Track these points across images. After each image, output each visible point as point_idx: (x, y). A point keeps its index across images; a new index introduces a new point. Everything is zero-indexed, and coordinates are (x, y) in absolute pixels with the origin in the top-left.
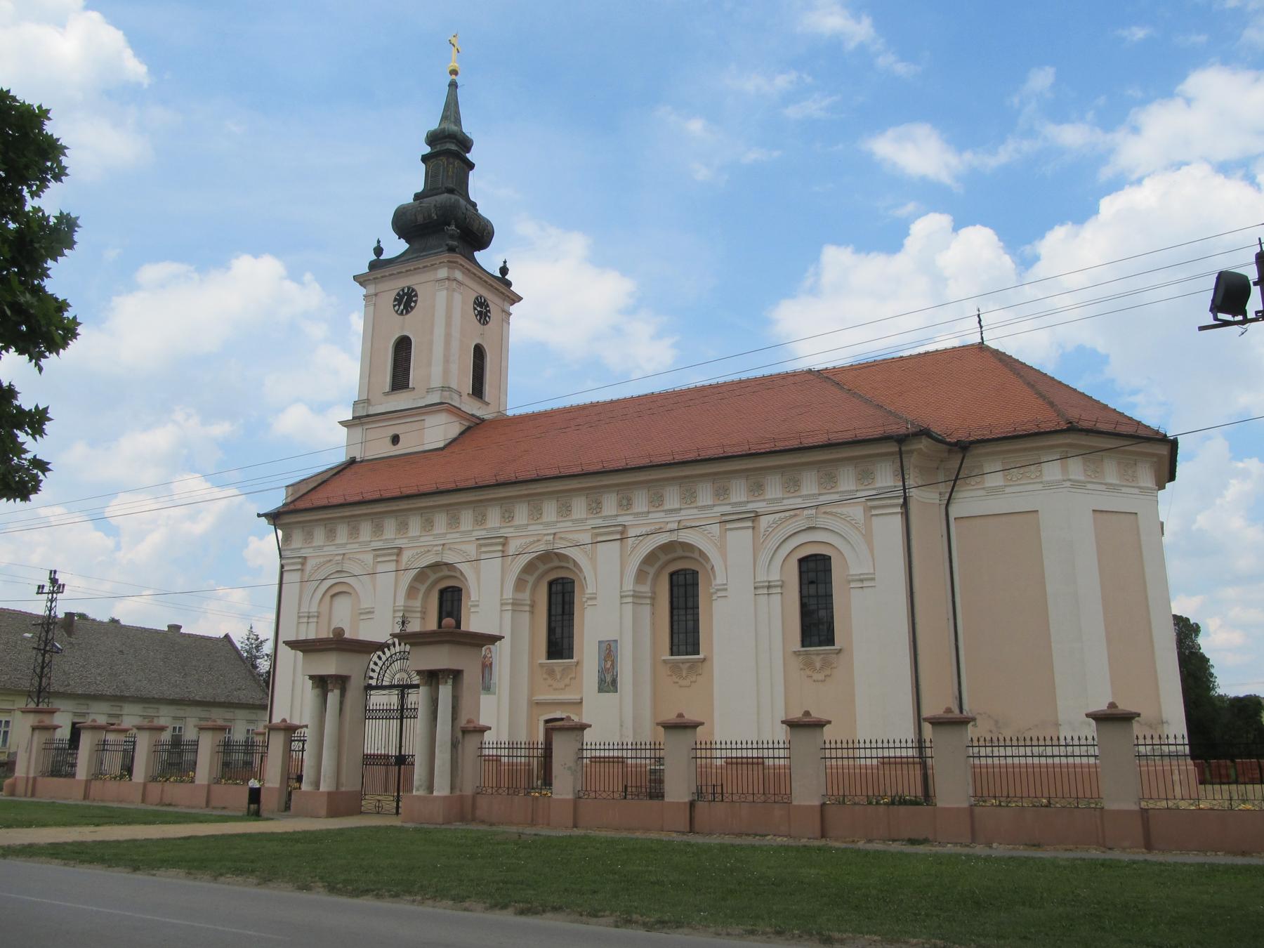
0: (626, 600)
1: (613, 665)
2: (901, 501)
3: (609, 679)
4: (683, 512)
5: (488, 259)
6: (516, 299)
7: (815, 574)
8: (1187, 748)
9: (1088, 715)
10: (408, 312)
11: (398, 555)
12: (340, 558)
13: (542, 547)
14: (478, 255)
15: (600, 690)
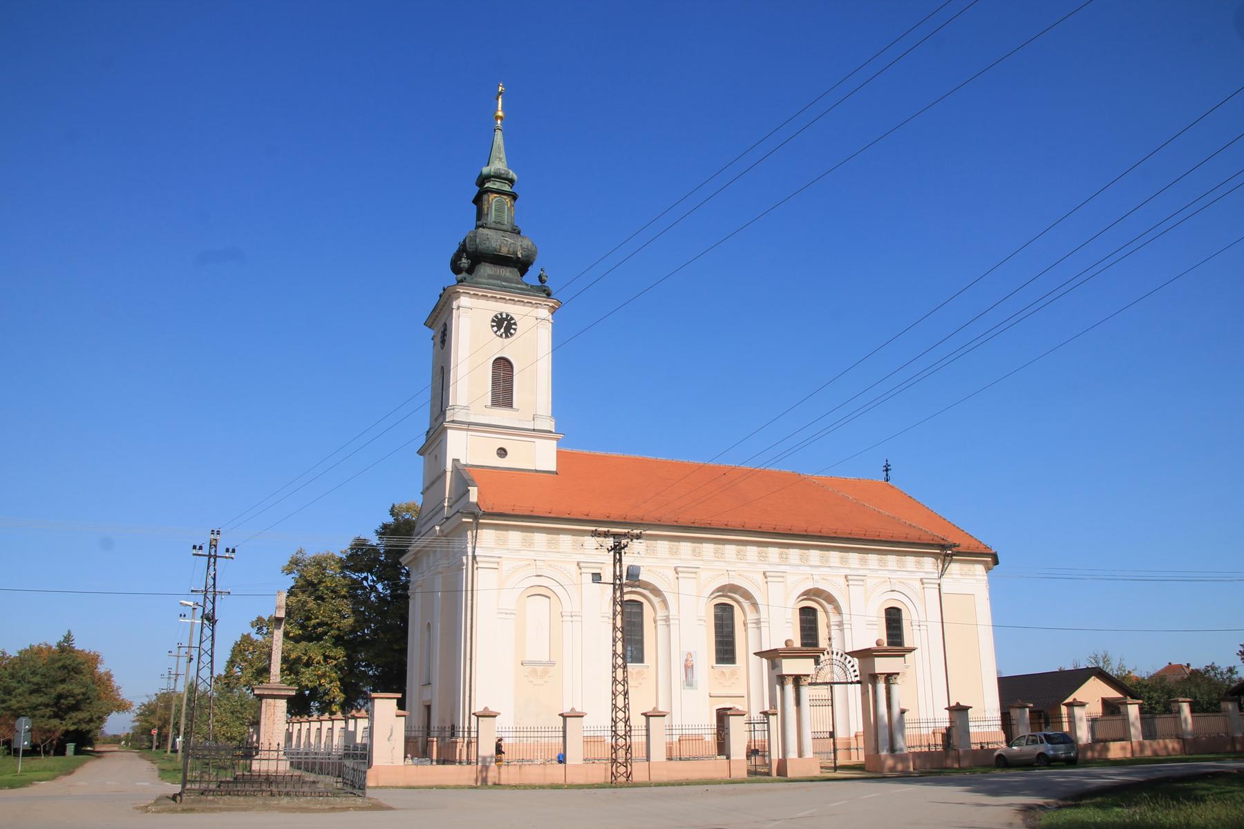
10: (507, 336)
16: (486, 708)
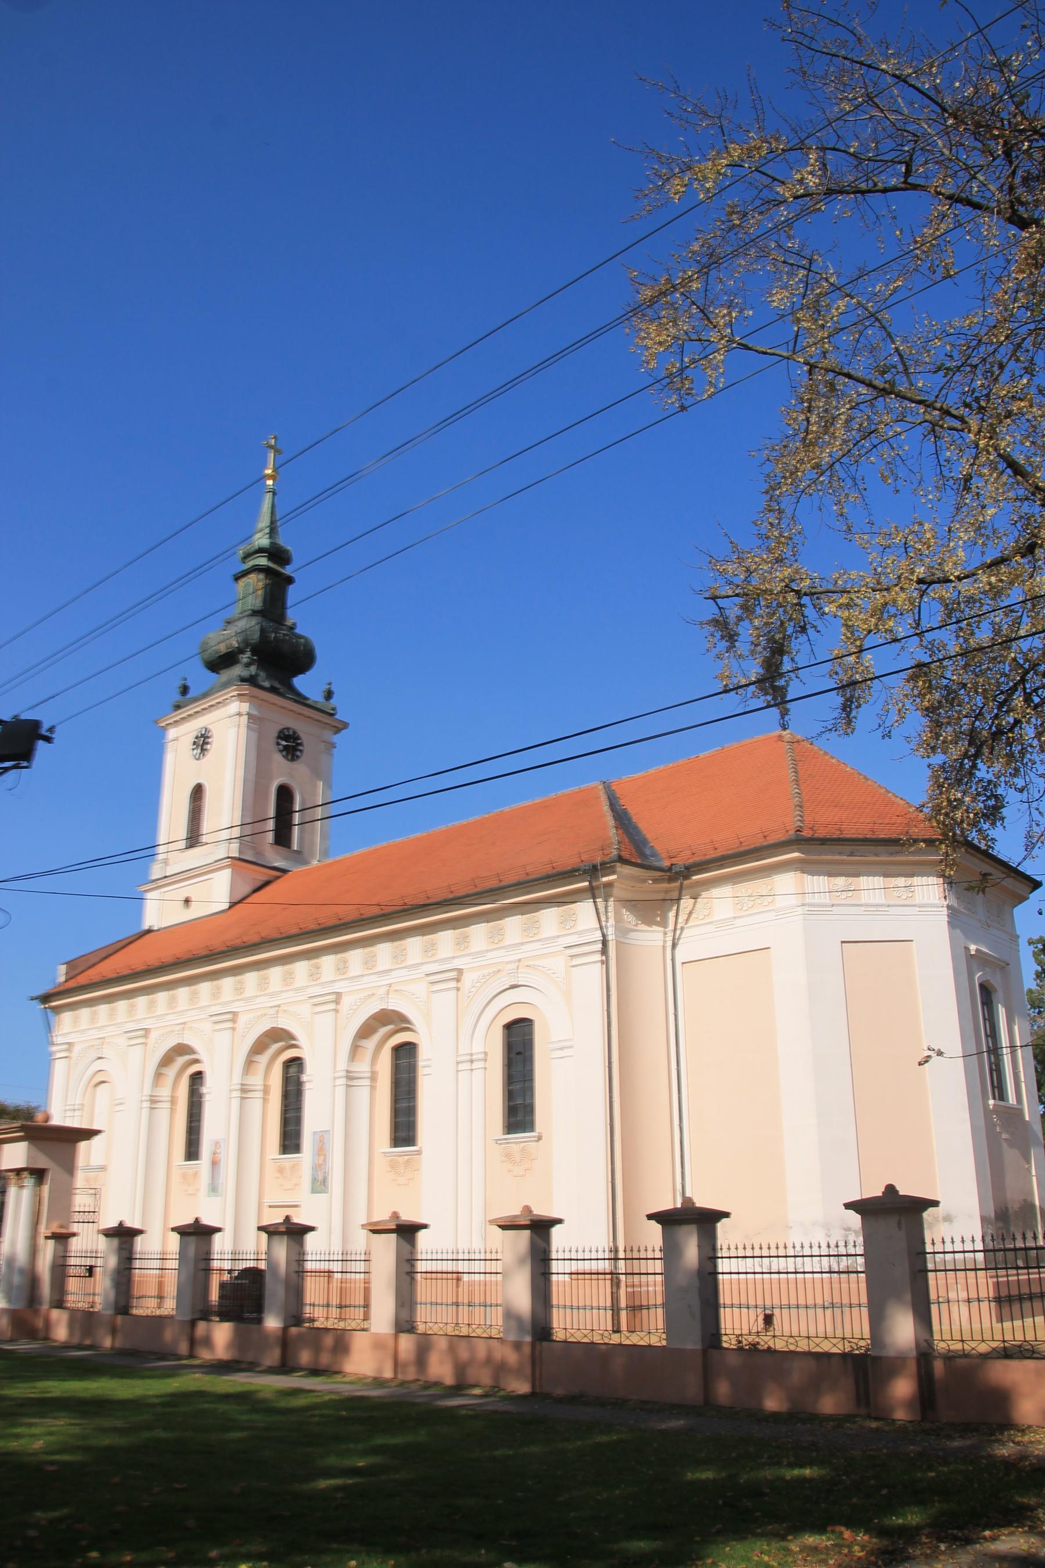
0: (461, 1067)
1: (324, 1160)
2: (599, 946)
3: (320, 1177)
4: (394, 974)
6: (340, 727)
7: (518, 1041)
8: (861, 1260)
9: (848, 1206)
11: (233, 1021)
12: (514, 966)
14: (300, 682)
15: (314, 1191)
16: (890, 1189)
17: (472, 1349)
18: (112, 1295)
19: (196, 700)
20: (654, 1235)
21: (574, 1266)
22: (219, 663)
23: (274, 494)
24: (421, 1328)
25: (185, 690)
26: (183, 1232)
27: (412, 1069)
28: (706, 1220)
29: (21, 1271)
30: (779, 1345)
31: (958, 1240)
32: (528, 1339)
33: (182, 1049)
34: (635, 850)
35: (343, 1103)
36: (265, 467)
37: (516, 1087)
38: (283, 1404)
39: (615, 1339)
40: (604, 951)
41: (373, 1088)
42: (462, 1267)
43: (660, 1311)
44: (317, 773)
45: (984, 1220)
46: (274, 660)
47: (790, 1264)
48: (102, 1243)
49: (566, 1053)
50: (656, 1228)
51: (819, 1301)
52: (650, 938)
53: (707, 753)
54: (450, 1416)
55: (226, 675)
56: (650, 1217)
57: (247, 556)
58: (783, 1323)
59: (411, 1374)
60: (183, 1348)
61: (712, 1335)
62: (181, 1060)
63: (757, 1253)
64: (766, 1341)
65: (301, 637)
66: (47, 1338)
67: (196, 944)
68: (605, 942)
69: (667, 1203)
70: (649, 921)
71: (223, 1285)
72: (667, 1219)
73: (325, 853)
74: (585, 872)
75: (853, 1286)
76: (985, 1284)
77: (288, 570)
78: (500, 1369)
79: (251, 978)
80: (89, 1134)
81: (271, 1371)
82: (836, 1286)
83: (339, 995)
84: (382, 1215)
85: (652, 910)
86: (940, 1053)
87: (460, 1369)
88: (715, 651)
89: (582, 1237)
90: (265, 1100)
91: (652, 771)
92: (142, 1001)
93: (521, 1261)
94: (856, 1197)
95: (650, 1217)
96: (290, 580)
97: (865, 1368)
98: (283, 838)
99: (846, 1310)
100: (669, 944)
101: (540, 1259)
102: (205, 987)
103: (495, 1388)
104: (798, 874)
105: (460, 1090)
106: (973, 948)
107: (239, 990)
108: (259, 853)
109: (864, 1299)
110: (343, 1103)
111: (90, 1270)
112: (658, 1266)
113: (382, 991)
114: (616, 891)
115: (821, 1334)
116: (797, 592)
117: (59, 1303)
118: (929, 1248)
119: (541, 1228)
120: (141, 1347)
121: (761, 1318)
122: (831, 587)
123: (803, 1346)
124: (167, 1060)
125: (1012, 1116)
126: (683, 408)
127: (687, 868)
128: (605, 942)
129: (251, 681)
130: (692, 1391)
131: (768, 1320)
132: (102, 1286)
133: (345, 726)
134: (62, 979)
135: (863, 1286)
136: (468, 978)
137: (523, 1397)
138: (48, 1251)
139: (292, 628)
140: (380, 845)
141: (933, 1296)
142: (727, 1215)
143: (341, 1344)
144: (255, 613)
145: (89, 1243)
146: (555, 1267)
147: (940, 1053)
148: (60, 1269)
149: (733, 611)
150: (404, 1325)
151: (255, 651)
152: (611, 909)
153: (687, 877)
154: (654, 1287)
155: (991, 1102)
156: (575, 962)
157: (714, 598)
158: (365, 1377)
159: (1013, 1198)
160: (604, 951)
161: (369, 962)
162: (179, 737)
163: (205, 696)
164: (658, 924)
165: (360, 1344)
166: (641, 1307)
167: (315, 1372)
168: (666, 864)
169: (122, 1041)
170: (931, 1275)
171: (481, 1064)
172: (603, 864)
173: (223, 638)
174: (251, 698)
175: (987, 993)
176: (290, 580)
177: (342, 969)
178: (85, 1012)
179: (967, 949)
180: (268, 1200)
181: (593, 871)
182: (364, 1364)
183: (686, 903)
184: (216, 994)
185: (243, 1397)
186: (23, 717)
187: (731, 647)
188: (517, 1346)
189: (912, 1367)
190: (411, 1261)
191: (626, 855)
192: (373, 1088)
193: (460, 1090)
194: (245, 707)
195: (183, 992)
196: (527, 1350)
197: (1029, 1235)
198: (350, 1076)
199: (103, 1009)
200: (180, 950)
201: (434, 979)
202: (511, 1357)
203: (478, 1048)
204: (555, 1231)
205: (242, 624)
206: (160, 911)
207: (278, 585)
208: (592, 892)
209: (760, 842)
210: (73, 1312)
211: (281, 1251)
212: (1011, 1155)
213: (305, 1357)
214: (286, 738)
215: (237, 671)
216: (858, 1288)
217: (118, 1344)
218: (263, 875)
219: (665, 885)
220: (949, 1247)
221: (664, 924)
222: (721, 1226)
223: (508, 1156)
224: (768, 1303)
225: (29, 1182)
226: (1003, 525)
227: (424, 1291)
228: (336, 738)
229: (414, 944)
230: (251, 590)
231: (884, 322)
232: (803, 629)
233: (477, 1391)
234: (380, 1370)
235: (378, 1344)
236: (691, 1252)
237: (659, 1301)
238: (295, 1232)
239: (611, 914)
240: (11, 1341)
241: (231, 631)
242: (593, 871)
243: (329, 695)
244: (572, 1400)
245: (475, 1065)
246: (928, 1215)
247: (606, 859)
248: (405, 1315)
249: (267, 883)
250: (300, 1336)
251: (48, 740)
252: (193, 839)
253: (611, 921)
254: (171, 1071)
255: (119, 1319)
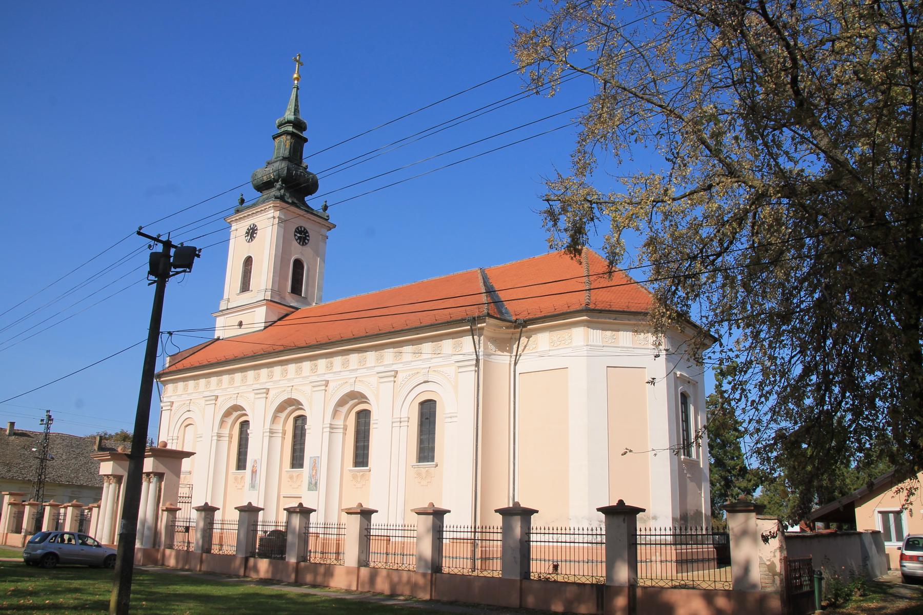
0: (394, 425)
2: (474, 362)
3: (314, 482)
5: (313, 201)
6: (332, 227)
7: (427, 413)
9: (599, 510)
13: (285, 397)
14: (309, 200)
15: (309, 489)
16: (621, 502)
17: (400, 577)
18: (200, 542)
19: (248, 207)
20: (498, 520)
21: (455, 535)
22: (263, 187)
23: (298, 89)
24: (372, 565)
25: (242, 201)
26: (241, 509)
27: (368, 424)
28: (527, 514)
29: (149, 528)
30: (560, 579)
31: (658, 529)
32: (430, 572)
33: (236, 408)
34: (496, 307)
35: (327, 442)
36: (294, 73)
37: (425, 437)
38: (301, 600)
39: (475, 574)
40: (477, 365)
41: (345, 434)
42: (391, 533)
43: (499, 561)
44: (317, 253)
45: (674, 519)
46: (294, 186)
47: (568, 538)
48: (194, 515)
49: (453, 419)
50: (499, 517)
51: (581, 559)
52: (503, 359)
53: (539, 256)
54: (390, 609)
55: (266, 194)
56: (496, 511)
57: (280, 125)
58: (562, 569)
59: (366, 589)
60: (242, 572)
61: (526, 574)
62: (235, 414)
63: (551, 532)
64: (553, 577)
65: (310, 174)
66: (163, 564)
67: (248, 349)
68: (478, 360)
69: (505, 504)
70: (503, 350)
71: (261, 539)
72: (505, 513)
73: (320, 299)
74: (468, 321)
75: (599, 551)
76: (671, 553)
77: (305, 134)
78: (414, 586)
79: (277, 370)
80: (189, 454)
81: (289, 584)
82: (595, 551)
83: (327, 382)
84: (353, 505)
85: (504, 344)
86: (631, 451)
87: (393, 586)
88: (547, 227)
89: (458, 521)
90: (283, 438)
91: (508, 264)
92: (214, 380)
93: (428, 531)
94: (606, 504)
95: (496, 511)
96: (306, 140)
97: (601, 592)
98: (296, 289)
99: (599, 564)
100: (513, 362)
101: (438, 532)
102: (251, 374)
103: (411, 597)
104: (586, 328)
105: (393, 437)
106: (678, 373)
107: (270, 376)
108: (283, 298)
109: (604, 559)
110: (327, 442)
111: (187, 529)
112: (500, 537)
113: (352, 381)
114: (485, 332)
115: (581, 574)
116: (590, 202)
117: (171, 547)
118: (638, 533)
119: (438, 514)
120: (221, 571)
121: (551, 567)
122: (607, 200)
123: (572, 579)
124: (227, 414)
125: (693, 465)
126: (537, 93)
127: (525, 322)
128: (478, 360)
129: (281, 198)
130: (514, 601)
131: (556, 567)
132: (195, 538)
133: (335, 226)
134: (167, 365)
135: (604, 552)
136: (400, 376)
137: (426, 601)
138: (164, 517)
139: (306, 168)
140: (351, 297)
141: (639, 559)
142: (537, 512)
143: (329, 571)
144: (284, 159)
145: (188, 514)
146: (445, 535)
147: (631, 451)
148: (171, 528)
149: (557, 206)
150: (363, 562)
151: (283, 182)
152: (482, 342)
153: (525, 326)
154: (496, 547)
155: (682, 457)
156: (460, 370)
157: (548, 200)
158: (341, 589)
159: (691, 508)
160: (477, 365)
161: (345, 364)
162: (239, 228)
163: (254, 205)
164: (507, 351)
165: (339, 572)
166: (489, 559)
167: (314, 586)
168: (514, 318)
169: (203, 402)
170: (639, 547)
171: (406, 424)
172: (479, 317)
173: (265, 173)
174: (281, 209)
175: (684, 397)
176: (306, 140)
177: (330, 367)
178: (181, 385)
179: (675, 374)
180: (283, 493)
181: (474, 321)
182: (342, 582)
183: (523, 340)
184: (257, 378)
185: (280, 597)
186: (185, 245)
187: (555, 224)
188: (424, 575)
189: (626, 590)
190: (368, 529)
191: (491, 312)
192: (345, 434)
193: (393, 437)
194: (277, 214)
195: (238, 376)
196: (429, 577)
197: (699, 528)
198: (332, 427)
199: (191, 383)
200: (237, 351)
201: (382, 375)
202: (421, 581)
203: (404, 415)
204: (446, 516)
205: (277, 165)
206: (225, 327)
207: (298, 142)
208: (472, 332)
209: (565, 310)
210: (178, 551)
211: (296, 521)
212: (691, 486)
213: (309, 578)
214: (300, 232)
215: (273, 192)
216: (601, 552)
217: (204, 568)
218: (285, 310)
219: (513, 330)
220: (653, 532)
221: (511, 351)
222: (534, 517)
223: (419, 474)
224: (555, 559)
225: (154, 480)
226: (697, 175)
227: (374, 546)
228: (328, 233)
229: (371, 356)
230: (283, 145)
231: (646, 58)
232: (592, 219)
233: (402, 598)
234: (350, 585)
235: (349, 571)
236: (518, 531)
237: (499, 555)
238: (305, 512)
239: (482, 345)
240: (143, 565)
241: (270, 169)
242: (474, 321)
243: (325, 208)
244: (452, 603)
245: (402, 424)
246: (639, 516)
247: (481, 314)
248: (363, 557)
249: (287, 315)
250: (306, 568)
251: (198, 256)
252: (245, 287)
253: (482, 349)
254: (230, 420)
255: (204, 555)
